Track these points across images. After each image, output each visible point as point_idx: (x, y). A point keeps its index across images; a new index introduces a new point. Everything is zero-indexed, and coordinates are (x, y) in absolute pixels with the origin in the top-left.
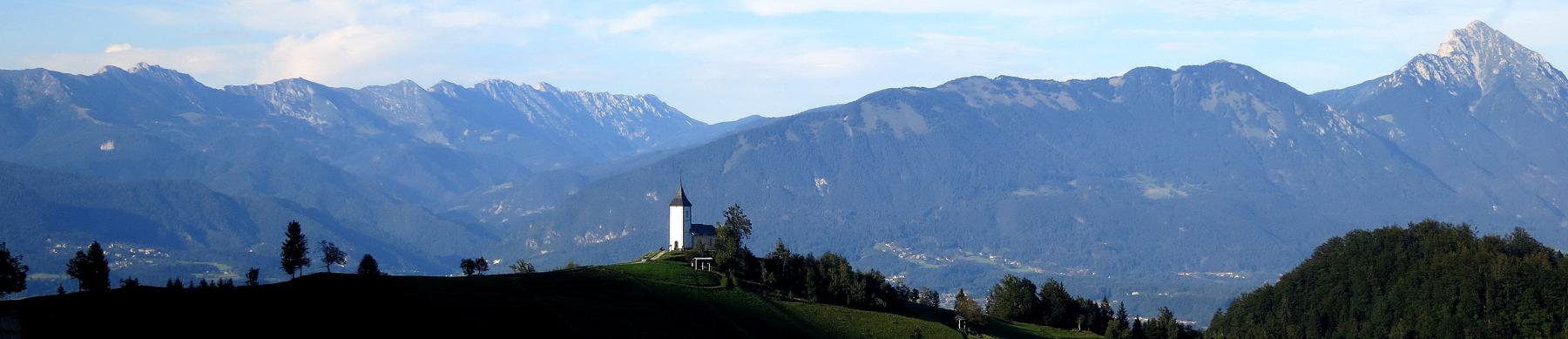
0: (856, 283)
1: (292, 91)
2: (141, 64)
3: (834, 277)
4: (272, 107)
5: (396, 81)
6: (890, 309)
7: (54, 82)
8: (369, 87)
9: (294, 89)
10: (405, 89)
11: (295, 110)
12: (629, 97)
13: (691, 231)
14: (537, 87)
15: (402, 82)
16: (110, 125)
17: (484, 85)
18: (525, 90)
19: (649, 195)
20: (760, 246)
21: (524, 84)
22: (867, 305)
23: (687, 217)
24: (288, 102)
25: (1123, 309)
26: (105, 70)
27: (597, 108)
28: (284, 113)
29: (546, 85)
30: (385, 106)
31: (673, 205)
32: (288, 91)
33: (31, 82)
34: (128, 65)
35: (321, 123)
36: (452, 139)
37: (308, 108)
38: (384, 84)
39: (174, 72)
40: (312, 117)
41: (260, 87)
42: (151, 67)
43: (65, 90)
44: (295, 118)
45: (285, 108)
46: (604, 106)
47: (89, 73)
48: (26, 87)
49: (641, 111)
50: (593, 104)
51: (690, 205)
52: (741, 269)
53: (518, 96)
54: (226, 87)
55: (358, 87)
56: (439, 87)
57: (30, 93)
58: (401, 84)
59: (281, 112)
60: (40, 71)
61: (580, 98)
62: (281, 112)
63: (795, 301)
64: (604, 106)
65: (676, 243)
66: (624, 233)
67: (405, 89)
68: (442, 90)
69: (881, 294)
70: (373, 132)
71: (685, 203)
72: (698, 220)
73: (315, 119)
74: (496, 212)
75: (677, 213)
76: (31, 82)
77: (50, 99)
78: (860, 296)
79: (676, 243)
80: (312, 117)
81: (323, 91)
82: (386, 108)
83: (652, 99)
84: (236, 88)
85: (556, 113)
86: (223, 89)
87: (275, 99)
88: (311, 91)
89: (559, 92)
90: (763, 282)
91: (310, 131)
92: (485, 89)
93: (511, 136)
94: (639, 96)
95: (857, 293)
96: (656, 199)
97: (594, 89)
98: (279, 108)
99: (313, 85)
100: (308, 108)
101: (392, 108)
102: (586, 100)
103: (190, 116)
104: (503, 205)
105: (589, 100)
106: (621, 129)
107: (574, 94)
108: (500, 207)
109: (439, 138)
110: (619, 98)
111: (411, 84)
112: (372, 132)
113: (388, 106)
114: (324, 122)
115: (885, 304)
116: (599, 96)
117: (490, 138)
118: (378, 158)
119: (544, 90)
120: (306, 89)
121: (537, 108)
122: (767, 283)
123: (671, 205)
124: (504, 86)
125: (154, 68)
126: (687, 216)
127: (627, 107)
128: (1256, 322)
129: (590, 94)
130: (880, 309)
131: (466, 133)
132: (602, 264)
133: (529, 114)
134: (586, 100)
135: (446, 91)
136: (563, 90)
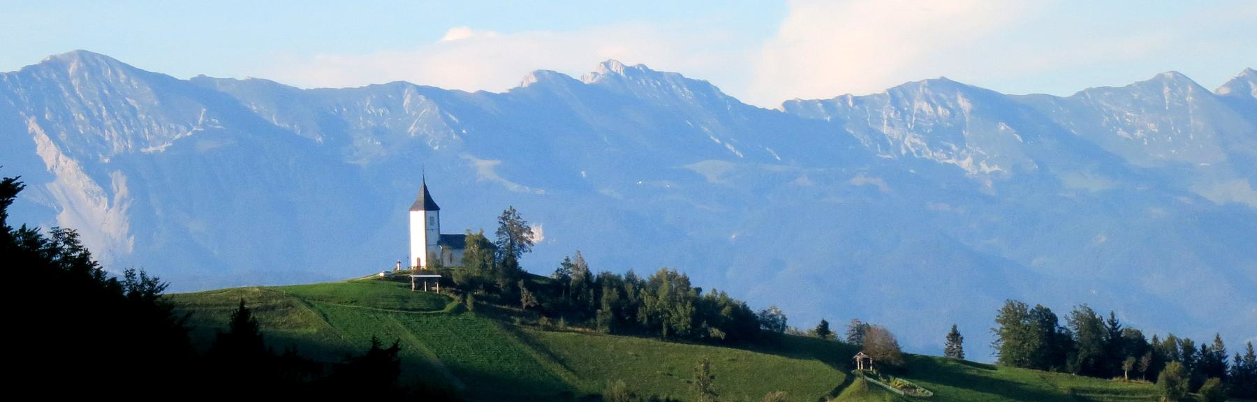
0: (679, 307)
1: (926, 107)
2: (607, 65)
3: (648, 300)
4: (883, 141)
5: (1148, 76)
6: (733, 340)
7: (428, 109)
9: (929, 102)
10: (1166, 90)
11: (933, 145)
15: (1161, 76)
16: (541, 191)
22: (695, 336)
23: (432, 224)
24: (918, 129)
26: (534, 80)
30: (1125, 129)
32: (917, 105)
33: (381, 111)
35: (988, 170)
37: (960, 141)
38: (1122, 84)
39: (678, 78)
40: (969, 160)
41: (857, 100)
42: (629, 70)
44: (931, 163)
45: (911, 142)
51: (435, 208)
55: (1065, 90)
57: (378, 132)
58: (1155, 84)
59: (904, 152)
60: (399, 87)
62: (904, 152)
63: (569, 331)
65: (419, 260)
67: (1166, 90)
71: (429, 205)
72: (448, 229)
73: (976, 163)
75: (417, 219)
76: (381, 111)
77: (419, 145)
78: (683, 325)
79: (419, 260)
80: (969, 160)
84: (808, 104)
86: (782, 110)
87: (891, 125)
88: (964, 104)
98: (898, 143)
99: (972, 93)
100: (960, 141)
101: (1139, 133)
103: (710, 169)
111: (1179, 81)
112: (1096, 185)
113: (1131, 130)
114: (996, 168)
115: (722, 335)
120: (955, 101)
125: (634, 72)
126: (430, 225)
130: (716, 342)
132: (1028, 370)
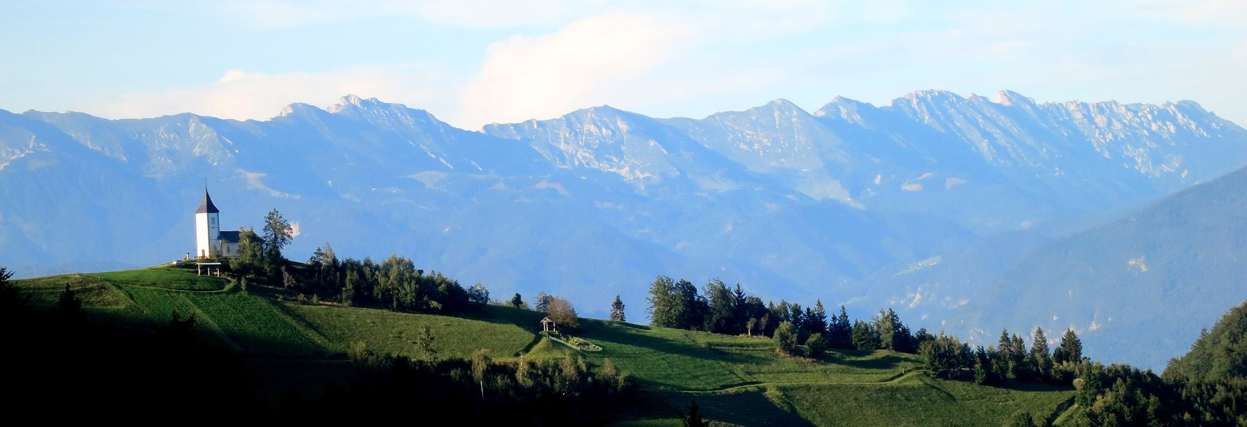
0: (406, 285)
1: (593, 129)
2: (347, 98)
3: (382, 280)
5: (762, 102)
7: (209, 134)
8: (718, 114)
9: (596, 125)
10: (777, 114)
11: (599, 157)
12: (1149, 106)
13: (219, 238)
14: (996, 99)
15: (772, 103)
17: (908, 101)
18: (978, 104)
19: (1132, 262)
20: (297, 251)
21: (974, 95)
22: (418, 307)
24: (587, 145)
25: (844, 314)
26: (290, 111)
27: (1097, 127)
28: (581, 164)
29: (1011, 94)
31: (199, 213)
32: (586, 127)
34: (328, 99)
35: (641, 176)
36: (856, 192)
37: (620, 154)
39: (402, 108)
40: (627, 168)
41: (540, 124)
42: (364, 102)
43: (226, 146)
44: (597, 172)
45: (583, 156)
46: (1110, 123)
47: (264, 116)
48: (164, 145)
49: (1172, 129)
50: (1091, 120)
51: (216, 211)
52: (265, 274)
53: (965, 116)
54: (486, 127)
55: (700, 115)
56: (833, 107)
57: (170, 153)
58: (769, 108)
60: (186, 118)
61: (1068, 113)
64: (1110, 123)
65: (203, 251)
66: (1094, 327)
68: (838, 111)
69: (434, 295)
70: (725, 187)
71: (211, 208)
72: (226, 227)
73: (632, 171)
74: (911, 305)
79: (203, 251)
80: (627, 168)
81: (643, 126)
82: (745, 147)
83: (1190, 109)
84: (502, 127)
85: (1030, 141)
86: (483, 132)
87: (567, 142)
88: (623, 126)
89: (1033, 106)
90: (283, 285)
91: (622, 191)
92: (910, 107)
93: (951, 182)
94: (1169, 104)
95: (406, 295)
96: (1144, 269)
97: (1092, 97)
100: (620, 154)
101: (756, 146)
102: (1078, 115)
103: (428, 178)
104: (922, 294)
105: (1085, 116)
106: (1139, 161)
107: (1058, 107)
108: (918, 296)
109: (834, 191)
110: (1135, 109)
111: (786, 106)
112: (725, 187)
113: (750, 144)
114: (647, 175)
115: (440, 306)
116: (1100, 109)
117: (915, 187)
118: (730, 229)
119: (1007, 103)
120: (615, 123)
121: (997, 133)
122: (289, 286)
123: (196, 213)
124: (940, 101)
126: (212, 224)
127: (1149, 124)
128: (1237, 342)
129: (1085, 105)
130: (435, 311)
131: (878, 180)
133: (984, 145)
134: (1078, 115)
135: (843, 113)
136: (1040, 101)
